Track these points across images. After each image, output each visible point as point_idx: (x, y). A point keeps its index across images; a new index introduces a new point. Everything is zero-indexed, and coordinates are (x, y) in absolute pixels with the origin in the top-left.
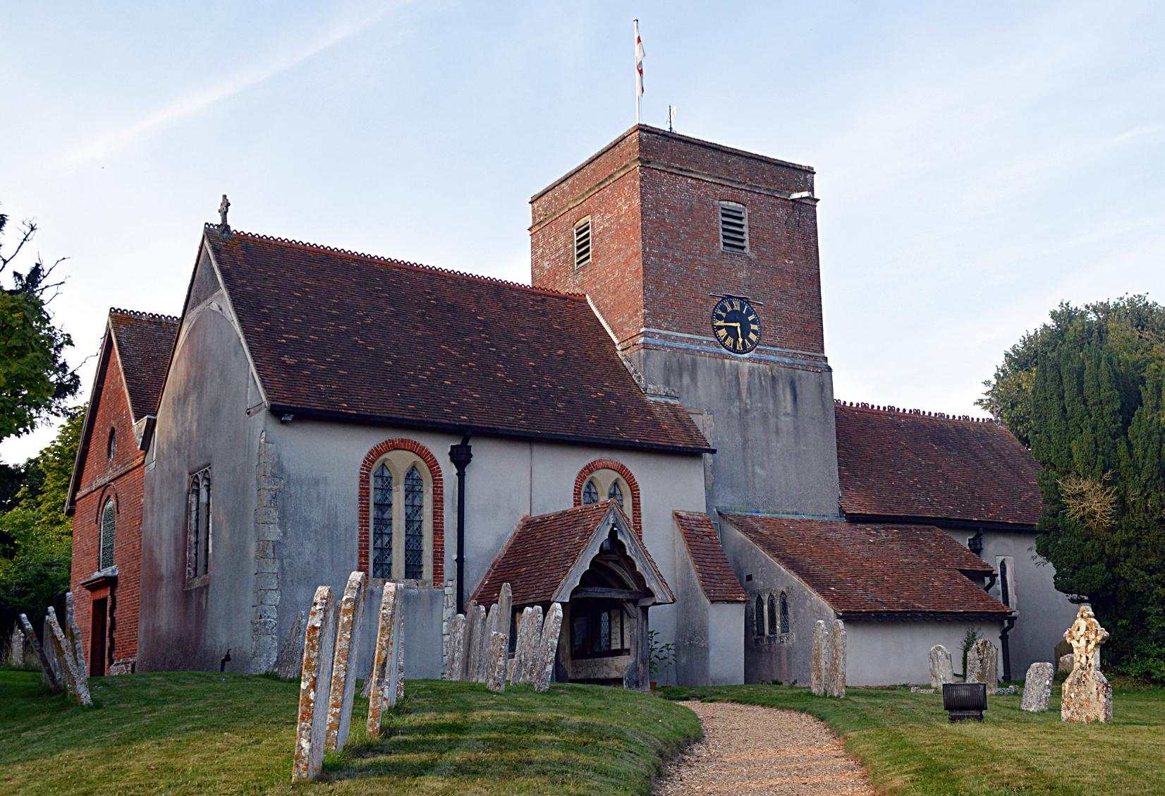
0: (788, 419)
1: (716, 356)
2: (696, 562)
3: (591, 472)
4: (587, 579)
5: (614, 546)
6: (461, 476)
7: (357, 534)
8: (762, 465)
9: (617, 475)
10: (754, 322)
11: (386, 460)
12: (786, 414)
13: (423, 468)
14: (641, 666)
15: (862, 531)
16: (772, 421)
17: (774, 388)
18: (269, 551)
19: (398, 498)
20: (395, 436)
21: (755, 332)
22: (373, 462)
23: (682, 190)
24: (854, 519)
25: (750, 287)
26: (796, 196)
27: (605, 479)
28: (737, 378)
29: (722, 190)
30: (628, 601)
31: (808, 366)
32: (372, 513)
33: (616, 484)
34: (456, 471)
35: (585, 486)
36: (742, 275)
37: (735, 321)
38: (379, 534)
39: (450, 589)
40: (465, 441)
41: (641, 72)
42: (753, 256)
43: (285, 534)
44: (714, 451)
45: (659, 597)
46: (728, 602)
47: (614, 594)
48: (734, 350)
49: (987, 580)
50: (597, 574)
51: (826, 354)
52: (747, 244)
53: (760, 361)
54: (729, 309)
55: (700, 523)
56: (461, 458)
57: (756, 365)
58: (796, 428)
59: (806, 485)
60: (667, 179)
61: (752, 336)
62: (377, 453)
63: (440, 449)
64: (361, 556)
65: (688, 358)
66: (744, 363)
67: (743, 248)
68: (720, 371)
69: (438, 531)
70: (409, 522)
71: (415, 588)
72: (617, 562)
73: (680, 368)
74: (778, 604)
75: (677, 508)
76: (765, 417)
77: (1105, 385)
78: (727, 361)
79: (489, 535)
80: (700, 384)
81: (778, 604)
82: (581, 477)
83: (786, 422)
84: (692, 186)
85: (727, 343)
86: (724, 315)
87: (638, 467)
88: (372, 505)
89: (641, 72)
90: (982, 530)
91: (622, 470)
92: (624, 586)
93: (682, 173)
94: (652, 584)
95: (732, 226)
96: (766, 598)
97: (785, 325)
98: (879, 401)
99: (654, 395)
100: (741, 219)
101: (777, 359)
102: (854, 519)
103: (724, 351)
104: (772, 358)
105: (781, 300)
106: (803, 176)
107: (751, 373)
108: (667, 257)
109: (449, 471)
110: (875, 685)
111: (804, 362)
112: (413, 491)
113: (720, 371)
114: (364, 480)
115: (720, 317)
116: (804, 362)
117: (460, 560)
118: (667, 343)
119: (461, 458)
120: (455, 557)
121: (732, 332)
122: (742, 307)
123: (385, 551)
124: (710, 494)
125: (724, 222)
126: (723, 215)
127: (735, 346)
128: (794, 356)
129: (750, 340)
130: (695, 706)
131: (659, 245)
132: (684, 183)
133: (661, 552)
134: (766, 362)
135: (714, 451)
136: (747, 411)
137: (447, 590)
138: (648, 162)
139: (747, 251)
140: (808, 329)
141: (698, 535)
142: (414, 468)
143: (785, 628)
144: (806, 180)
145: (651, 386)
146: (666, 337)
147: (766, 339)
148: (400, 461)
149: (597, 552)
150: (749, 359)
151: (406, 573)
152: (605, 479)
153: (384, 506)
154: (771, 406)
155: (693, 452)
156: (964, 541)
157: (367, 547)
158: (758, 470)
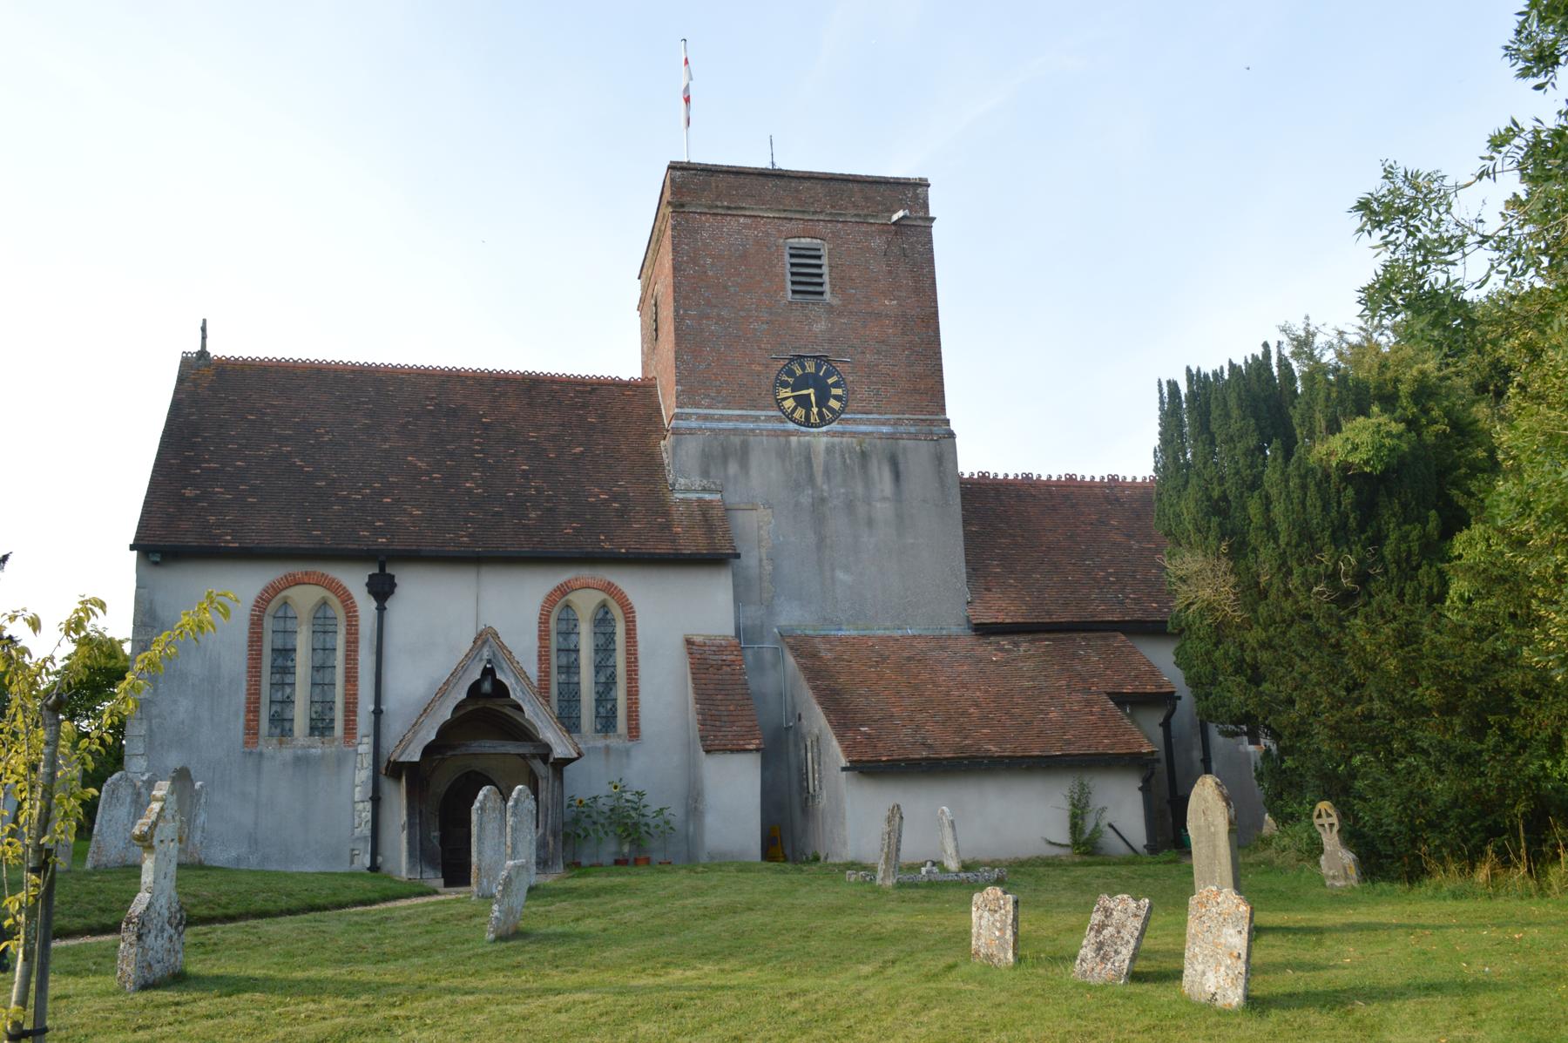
0: (887, 505)
1: (775, 434)
2: (698, 701)
3: (565, 594)
6: (381, 609)
7: (244, 685)
9: (601, 596)
10: (836, 385)
11: (286, 597)
12: (884, 499)
13: (335, 602)
14: (550, 840)
15: (992, 650)
20: (297, 569)
21: (838, 398)
22: (268, 602)
23: (731, 232)
24: (984, 630)
25: (831, 341)
26: (895, 217)
27: (585, 603)
28: (809, 460)
29: (789, 225)
30: (534, 756)
31: (916, 434)
34: (374, 604)
36: (820, 327)
37: (814, 386)
39: (365, 747)
40: (382, 569)
41: (687, 100)
42: (836, 302)
43: (155, 690)
46: (732, 751)
48: (807, 423)
51: (948, 416)
52: (827, 288)
54: (799, 372)
55: (721, 649)
56: (382, 590)
57: (836, 440)
59: (909, 590)
60: (708, 221)
61: (833, 403)
62: (271, 592)
63: (355, 580)
64: (249, 711)
65: (736, 440)
66: (820, 439)
67: (821, 293)
68: (783, 453)
69: (351, 677)
71: (318, 748)
73: (726, 453)
76: (850, 506)
77: (1235, 413)
78: (794, 439)
80: (754, 472)
83: (883, 510)
84: (746, 226)
85: (797, 415)
86: (791, 380)
87: (638, 587)
89: (687, 100)
91: (609, 588)
93: (732, 211)
95: (806, 271)
97: (884, 383)
98: (1049, 466)
99: (687, 490)
100: (819, 257)
101: (869, 428)
102: (984, 630)
103: (791, 426)
104: (863, 428)
105: (879, 353)
106: (912, 191)
107: (830, 450)
108: (708, 318)
109: (366, 606)
110: (1004, 855)
111: (912, 429)
114: (544, 621)
115: (785, 385)
116: (912, 429)
118: (708, 425)
119: (382, 590)
120: (372, 707)
121: (803, 402)
122: (819, 367)
125: (793, 265)
126: (792, 256)
127: (807, 417)
128: (897, 423)
129: (831, 409)
131: (698, 305)
132: (732, 224)
134: (853, 434)
136: (823, 500)
137: (361, 749)
138: (682, 206)
139: (827, 296)
140: (926, 388)
142: (324, 603)
144: (916, 196)
145: (682, 481)
146: (706, 418)
147: (853, 405)
148: (305, 598)
149: (463, 696)
150: (827, 433)
152: (585, 603)
154: (860, 490)
155: (715, 559)
157: (257, 701)
158: (840, 575)
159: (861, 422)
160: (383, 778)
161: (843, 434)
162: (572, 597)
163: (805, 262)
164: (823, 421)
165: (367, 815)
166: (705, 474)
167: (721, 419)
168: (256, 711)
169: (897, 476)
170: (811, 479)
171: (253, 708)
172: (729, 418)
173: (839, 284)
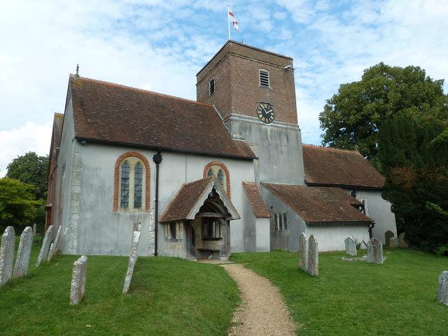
4: (203, 209)
5: (214, 195)
6: (158, 167)
8: (276, 165)
16: (279, 148)
17: (280, 136)
18: (75, 197)
19: (132, 176)
24: (310, 185)
27: (216, 169)
28: (266, 132)
32: (120, 182)
33: (220, 171)
35: (209, 172)
38: (123, 190)
39: (152, 213)
40: (159, 153)
44: (257, 159)
45: (234, 216)
47: (215, 215)
48: (265, 122)
49: (360, 208)
50: (207, 207)
53: (274, 126)
56: (158, 160)
58: (289, 151)
66: (268, 127)
68: (260, 130)
70: (136, 186)
71: (137, 212)
72: (217, 202)
73: (245, 128)
74: (283, 218)
75: (244, 180)
76: (276, 147)
79: (169, 191)
81: (283, 218)
82: (206, 168)
83: (284, 149)
88: (120, 178)
90: (356, 189)
91: (222, 166)
92: (220, 212)
94: (231, 211)
96: (278, 216)
102: (310, 185)
107: (272, 131)
109: (152, 165)
112: (138, 172)
113: (260, 130)
114: (117, 169)
117: (157, 201)
119: (158, 160)
123: (126, 197)
124: (257, 174)
130: (264, 200)
133: (237, 201)
135: (257, 159)
141: (249, 190)
142: (139, 163)
143: (286, 227)
146: (240, 117)
148: (133, 161)
151: (135, 206)
152: (216, 169)
153: (126, 179)
155: (249, 159)
156: (350, 193)
157: (117, 195)
158: (274, 166)
159: (278, 123)
160: (159, 225)
161: (274, 126)
162: (212, 167)
163: (264, 75)
164: (269, 122)
165: (154, 236)
166: (241, 134)
167: (244, 118)
168: (117, 199)
169: (287, 140)
170: (267, 138)
171: (116, 198)
172: (246, 118)
173: (273, 83)
